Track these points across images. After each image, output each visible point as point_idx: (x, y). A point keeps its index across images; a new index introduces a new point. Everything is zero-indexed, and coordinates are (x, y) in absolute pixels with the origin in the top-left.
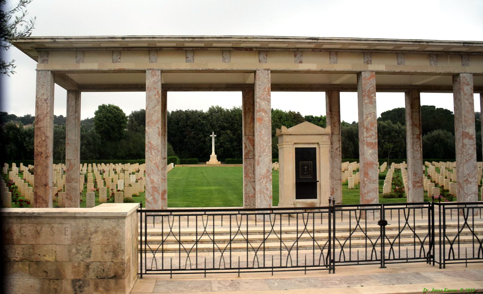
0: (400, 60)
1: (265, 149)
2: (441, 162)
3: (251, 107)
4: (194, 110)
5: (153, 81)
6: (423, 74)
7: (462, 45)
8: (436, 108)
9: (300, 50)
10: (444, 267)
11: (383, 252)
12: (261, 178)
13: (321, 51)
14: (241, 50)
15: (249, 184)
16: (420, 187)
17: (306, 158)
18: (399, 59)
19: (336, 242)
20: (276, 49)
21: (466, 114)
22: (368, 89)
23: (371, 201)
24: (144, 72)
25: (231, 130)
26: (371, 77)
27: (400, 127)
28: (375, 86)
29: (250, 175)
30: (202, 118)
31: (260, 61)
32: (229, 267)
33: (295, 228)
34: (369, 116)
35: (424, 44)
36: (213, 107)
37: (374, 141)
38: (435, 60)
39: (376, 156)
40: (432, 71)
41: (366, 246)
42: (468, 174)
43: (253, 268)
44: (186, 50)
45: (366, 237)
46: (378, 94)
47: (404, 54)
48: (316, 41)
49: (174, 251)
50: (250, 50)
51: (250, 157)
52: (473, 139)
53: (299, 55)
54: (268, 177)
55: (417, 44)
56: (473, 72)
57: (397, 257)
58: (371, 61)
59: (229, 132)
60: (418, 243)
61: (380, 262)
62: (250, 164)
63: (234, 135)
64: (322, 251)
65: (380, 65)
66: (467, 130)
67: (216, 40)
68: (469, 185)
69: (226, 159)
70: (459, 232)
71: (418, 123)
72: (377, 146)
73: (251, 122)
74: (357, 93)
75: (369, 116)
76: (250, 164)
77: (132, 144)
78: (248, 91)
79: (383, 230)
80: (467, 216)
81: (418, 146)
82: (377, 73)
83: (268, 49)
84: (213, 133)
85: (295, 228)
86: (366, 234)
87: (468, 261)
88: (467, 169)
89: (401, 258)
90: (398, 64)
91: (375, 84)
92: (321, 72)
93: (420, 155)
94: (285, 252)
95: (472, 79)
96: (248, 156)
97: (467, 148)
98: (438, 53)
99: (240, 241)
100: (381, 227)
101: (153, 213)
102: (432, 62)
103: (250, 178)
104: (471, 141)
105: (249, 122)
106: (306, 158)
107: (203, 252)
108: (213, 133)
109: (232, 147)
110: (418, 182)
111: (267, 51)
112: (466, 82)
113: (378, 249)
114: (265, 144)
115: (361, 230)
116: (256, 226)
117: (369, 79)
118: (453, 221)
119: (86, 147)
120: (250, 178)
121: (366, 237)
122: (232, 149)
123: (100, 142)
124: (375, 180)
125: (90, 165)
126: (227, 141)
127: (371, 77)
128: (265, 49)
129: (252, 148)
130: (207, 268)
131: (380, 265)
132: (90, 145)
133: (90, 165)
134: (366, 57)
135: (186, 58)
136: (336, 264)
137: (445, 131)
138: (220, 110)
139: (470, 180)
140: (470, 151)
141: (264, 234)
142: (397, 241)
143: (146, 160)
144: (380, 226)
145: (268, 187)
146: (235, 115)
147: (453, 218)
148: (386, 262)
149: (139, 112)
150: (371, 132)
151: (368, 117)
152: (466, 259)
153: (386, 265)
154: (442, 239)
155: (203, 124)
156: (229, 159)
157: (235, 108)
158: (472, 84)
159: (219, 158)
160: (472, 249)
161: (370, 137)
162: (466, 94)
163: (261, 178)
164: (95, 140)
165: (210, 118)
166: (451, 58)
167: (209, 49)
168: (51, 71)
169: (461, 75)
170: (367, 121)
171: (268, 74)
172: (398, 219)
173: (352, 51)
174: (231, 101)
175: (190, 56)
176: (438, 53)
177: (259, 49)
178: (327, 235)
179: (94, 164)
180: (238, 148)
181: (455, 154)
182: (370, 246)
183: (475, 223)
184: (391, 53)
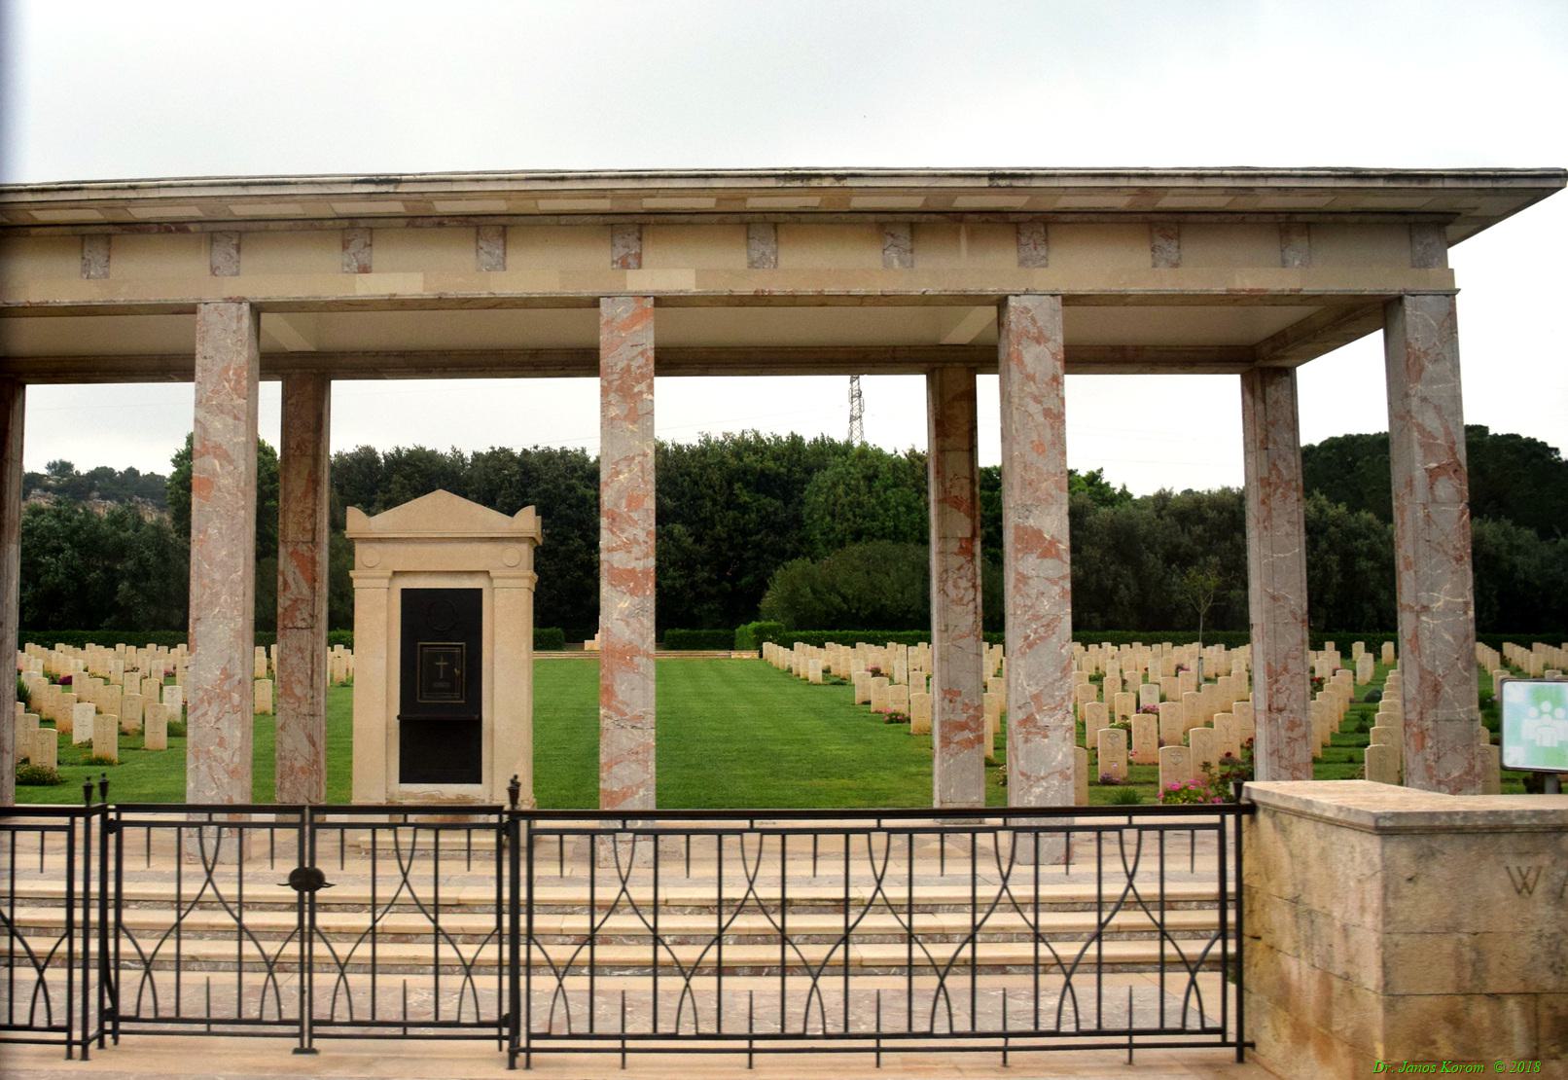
0: (760, 249)
1: (217, 595)
2: (151, 647)
3: (308, 436)
4: (556, 447)
5: (628, 341)
6: (862, 300)
7: (985, 183)
8: (1491, 432)
9: (362, 223)
10: (528, 1066)
11: (306, 993)
12: (202, 701)
13: (440, 225)
14: (148, 232)
16: (970, 744)
17: (441, 627)
18: (755, 243)
19: (126, 946)
20: (272, 225)
21: (1032, 457)
22: (621, 365)
23: (625, 796)
26: (635, 319)
27: (1321, 511)
28: (651, 354)
29: (298, 690)
30: (582, 478)
31: (213, 271)
32: (586, 1030)
33: (584, 893)
34: (622, 466)
35: (826, 183)
37: (639, 565)
39: (649, 622)
40: (890, 288)
41: (240, 964)
42: (1036, 697)
43: (674, 1037)
44: (1017, 224)
45: (242, 932)
46: (664, 385)
47: (775, 225)
48: (390, 188)
49: (885, 968)
50: (178, 230)
52: (1058, 556)
53: (356, 245)
54: (224, 697)
55: (798, 184)
56: (1064, 289)
57: (962, 1024)
58: (639, 257)
60: (666, 966)
61: (296, 1029)
62: (300, 650)
63: (699, 540)
64: (942, 979)
65: (673, 270)
66: (1031, 522)
67: (239, 191)
70: (975, 928)
71: (966, 494)
72: (651, 585)
73: (305, 496)
74: (996, 377)
75: (622, 466)
76: (300, 650)
78: (951, 374)
79: (306, 906)
81: (964, 583)
82: (660, 301)
83: (241, 226)
85: (1092, 891)
86: (239, 919)
87: (884, 1043)
88: (1029, 676)
89: (378, 1018)
90: (752, 265)
91: (650, 344)
92: (440, 303)
93: (971, 619)
94: (26, 974)
95: (1059, 318)
97: (1034, 592)
98: (915, 218)
99: (813, 938)
100: (301, 897)
101: (1034, 822)
102: (893, 255)
103: (299, 700)
104: (1049, 562)
106: (441, 627)
107: (1005, 973)
110: (962, 727)
111: (240, 233)
112: (1034, 331)
113: (289, 982)
114: (217, 576)
115: (222, 903)
116: (942, 876)
117: (627, 325)
118: (1200, 880)
119: (132, 586)
121: (373, 934)
124: (640, 718)
126: (672, 565)
127: (635, 319)
128: (232, 226)
129: (306, 591)
130: (756, 1031)
131: (295, 1043)
132: (147, 576)
134: (619, 242)
135: (1153, 250)
136: (123, 1026)
137: (1508, 523)
139: (1042, 719)
140: (1045, 606)
141: (1100, 911)
142: (169, 948)
144: (295, 893)
145: (225, 733)
146: (704, 468)
147: (948, 870)
148: (317, 1030)
149: (351, 456)
150: (631, 532)
151: (618, 473)
152: (623, 1037)
153: (317, 1043)
154: (78, 947)
157: (707, 441)
158: (1060, 339)
160: (778, 1002)
161: (627, 547)
162: (1030, 378)
163: (202, 701)
164: (166, 561)
166: (972, 236)
167: (34, 231)
168: (252, 305)
170: (616, 485)
171: (240, 318)
172: (1095, 869)
173: (563, 220)
174: (893, 415)
175: (97, 255)
176: (915, 218)
177: (210, 227)
178: (60, 914)
180: (713, 590)
181: (536, 612)
182: (326, 968)
183: (918, 892)
184: (722, 223)
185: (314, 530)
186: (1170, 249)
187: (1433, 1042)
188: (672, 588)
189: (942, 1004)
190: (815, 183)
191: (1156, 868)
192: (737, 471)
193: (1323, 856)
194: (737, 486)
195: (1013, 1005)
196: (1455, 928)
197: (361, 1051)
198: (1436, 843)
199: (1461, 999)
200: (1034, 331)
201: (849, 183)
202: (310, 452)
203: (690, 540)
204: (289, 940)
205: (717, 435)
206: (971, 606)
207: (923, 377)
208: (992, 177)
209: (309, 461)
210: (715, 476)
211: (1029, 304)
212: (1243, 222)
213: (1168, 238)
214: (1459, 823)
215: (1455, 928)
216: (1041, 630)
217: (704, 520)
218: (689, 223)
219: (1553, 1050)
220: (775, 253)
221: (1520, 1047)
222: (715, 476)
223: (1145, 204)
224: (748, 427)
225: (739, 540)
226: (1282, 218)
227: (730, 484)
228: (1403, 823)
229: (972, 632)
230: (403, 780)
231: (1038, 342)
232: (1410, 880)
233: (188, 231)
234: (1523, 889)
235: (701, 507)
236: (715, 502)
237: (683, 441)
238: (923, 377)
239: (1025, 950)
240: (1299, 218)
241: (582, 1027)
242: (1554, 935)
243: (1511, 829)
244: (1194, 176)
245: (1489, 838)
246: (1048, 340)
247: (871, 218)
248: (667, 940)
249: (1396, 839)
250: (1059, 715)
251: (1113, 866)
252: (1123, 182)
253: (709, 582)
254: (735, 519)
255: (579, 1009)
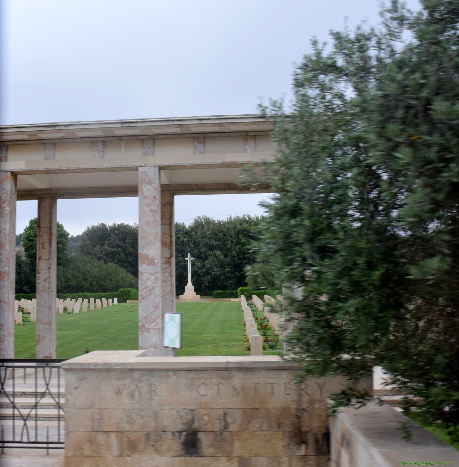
2: (68, 300)
6: (87, 170)
7: (119, 125)
24: (136, 169)
25: (221, 250)
35: (62, 128)
36: (249, 216)
38: (100, 148)
42: (145, 318)
47: (54, 144)
55: (51, 129)
59: (218, 252)
63: (226, 256)
68: (145, 333)
69: (215, 292)
77: (71, 272)
80: (50, 378)
84: (189, 254)
90: (46, 158)
97: (145, 278)
98: (104, 139)
108: (189, 254)
109: (224, 274)
112: (147, 180)
122: (223, 277)
123: (28, 270)
125: (86, 300)
133: (98, 300)
135: (194, 148)
138: (208, 222)
142: (33, 412)
143: (37, 295)
146: (228, 229)
147: (27, 382)
149: (97, 227)
155: (183, 242)
156: (218, 291)
157: (230, 218)
158: (157, 182)
159: (198, 290)
165: (193, 233)
168: (12, 173)
169: (140, 169)
176: (104, 139)
179: (104, 299)
180: (232, 276)
186: (200, 147)
187: (83, 449)
188: (216, 275)
189: (25, 431)
190: (57, 128)
191: (57, 383)
192: (241, 230)
194: (240, 236)
195: (51, 433)
196: (92, 407)
198: (86, 374)
199: (93, 433)
200: (147, 180)
201: (70, 127)
203: (223, 257)
204: (33, 408)
205: (233, 216)
206: (170, 283)
207: (58, 200)
208: (122, 123)
210: (233, 232)
211: (146, 170)
212: (229, 136)
213: (199, 143)
214: (93, 367)
215: (92, 407)
216: (148, 293)
217: (228, 249)
218: (23, 144)
219: (128, 453)
220: (54, 153)
221: (116, 452)
222: (233, 232)
223: (184, 131)
224: (246, 214)
225: (241, 256)
226: (244, 134)
227: (238, 235)
228: (257, 366)
229: (171, 293)
231: (149, 184)
232: (76, 388)
234: (119, 392)
235: (227, 244)
236: (232, 242)
237: (221, 219)
238: (58, 200)
239: (54, 412)
240: (251, 134)
241: (33, 439)
242: (130, 410)
243: (114, 370)
244: (198, 119)
245: (106, 373)
246: (152, 183)
247: (88, 139)
248: (17, 406)
249: (72, 372)
250: (154, 324)
251: (41, 382)
252: (171, 123)
253: (231, 272)
254: (240, 248)
255: (32, 433)
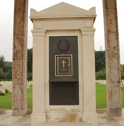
3: (22, 6)
15: (16, 86)
51: (20, 58)
73: (20, 22)
76: (19, 65)
96: (17, 56)
103: (18, 79)
105: (19, 21)
120: (18, 79)
129: (21, 49)
185: (23, 31)
193: (106, 111)
197: (53, 112)
202: (22, 10)
209: (22, 13)
230: (50, 104)
233: (59, 120)
